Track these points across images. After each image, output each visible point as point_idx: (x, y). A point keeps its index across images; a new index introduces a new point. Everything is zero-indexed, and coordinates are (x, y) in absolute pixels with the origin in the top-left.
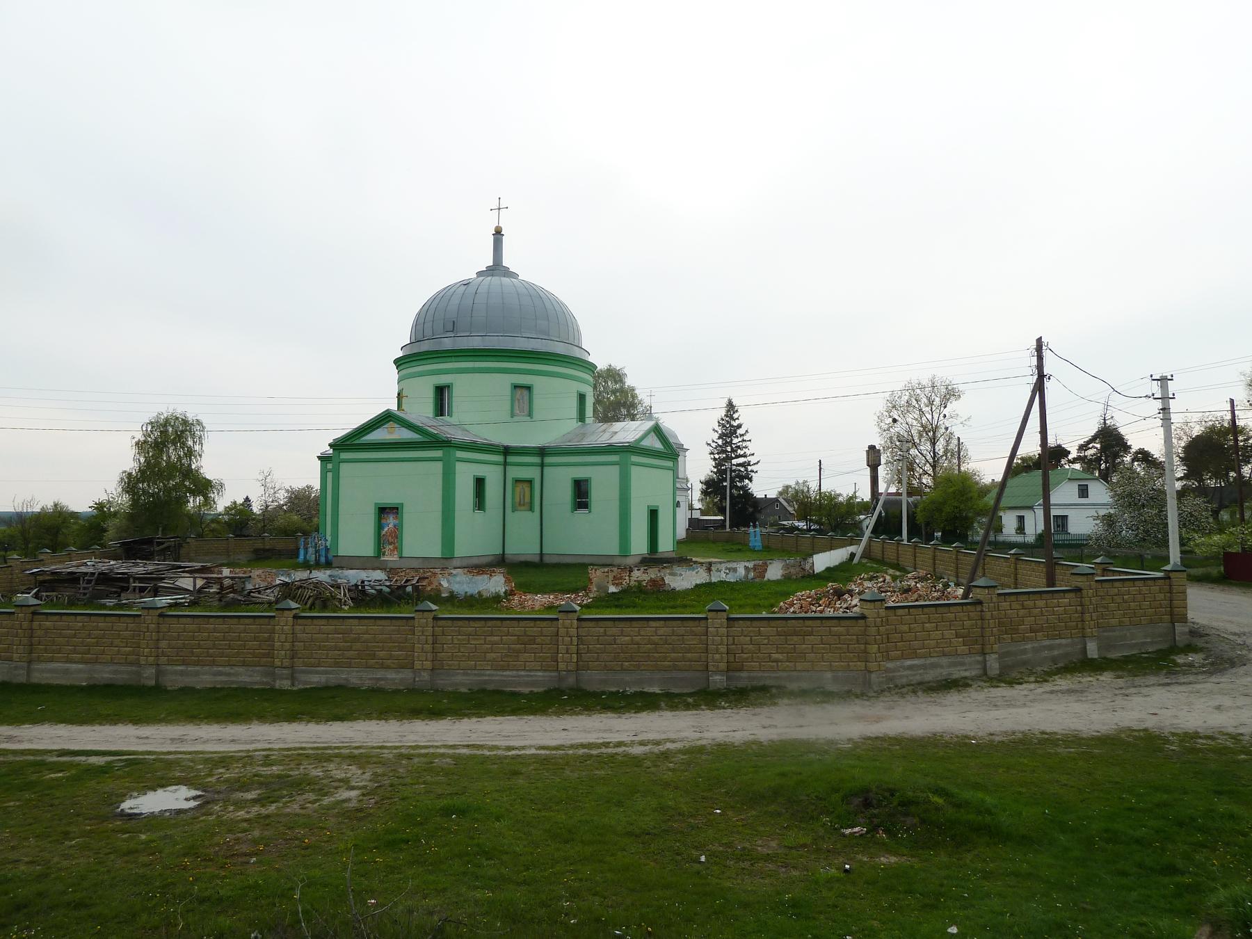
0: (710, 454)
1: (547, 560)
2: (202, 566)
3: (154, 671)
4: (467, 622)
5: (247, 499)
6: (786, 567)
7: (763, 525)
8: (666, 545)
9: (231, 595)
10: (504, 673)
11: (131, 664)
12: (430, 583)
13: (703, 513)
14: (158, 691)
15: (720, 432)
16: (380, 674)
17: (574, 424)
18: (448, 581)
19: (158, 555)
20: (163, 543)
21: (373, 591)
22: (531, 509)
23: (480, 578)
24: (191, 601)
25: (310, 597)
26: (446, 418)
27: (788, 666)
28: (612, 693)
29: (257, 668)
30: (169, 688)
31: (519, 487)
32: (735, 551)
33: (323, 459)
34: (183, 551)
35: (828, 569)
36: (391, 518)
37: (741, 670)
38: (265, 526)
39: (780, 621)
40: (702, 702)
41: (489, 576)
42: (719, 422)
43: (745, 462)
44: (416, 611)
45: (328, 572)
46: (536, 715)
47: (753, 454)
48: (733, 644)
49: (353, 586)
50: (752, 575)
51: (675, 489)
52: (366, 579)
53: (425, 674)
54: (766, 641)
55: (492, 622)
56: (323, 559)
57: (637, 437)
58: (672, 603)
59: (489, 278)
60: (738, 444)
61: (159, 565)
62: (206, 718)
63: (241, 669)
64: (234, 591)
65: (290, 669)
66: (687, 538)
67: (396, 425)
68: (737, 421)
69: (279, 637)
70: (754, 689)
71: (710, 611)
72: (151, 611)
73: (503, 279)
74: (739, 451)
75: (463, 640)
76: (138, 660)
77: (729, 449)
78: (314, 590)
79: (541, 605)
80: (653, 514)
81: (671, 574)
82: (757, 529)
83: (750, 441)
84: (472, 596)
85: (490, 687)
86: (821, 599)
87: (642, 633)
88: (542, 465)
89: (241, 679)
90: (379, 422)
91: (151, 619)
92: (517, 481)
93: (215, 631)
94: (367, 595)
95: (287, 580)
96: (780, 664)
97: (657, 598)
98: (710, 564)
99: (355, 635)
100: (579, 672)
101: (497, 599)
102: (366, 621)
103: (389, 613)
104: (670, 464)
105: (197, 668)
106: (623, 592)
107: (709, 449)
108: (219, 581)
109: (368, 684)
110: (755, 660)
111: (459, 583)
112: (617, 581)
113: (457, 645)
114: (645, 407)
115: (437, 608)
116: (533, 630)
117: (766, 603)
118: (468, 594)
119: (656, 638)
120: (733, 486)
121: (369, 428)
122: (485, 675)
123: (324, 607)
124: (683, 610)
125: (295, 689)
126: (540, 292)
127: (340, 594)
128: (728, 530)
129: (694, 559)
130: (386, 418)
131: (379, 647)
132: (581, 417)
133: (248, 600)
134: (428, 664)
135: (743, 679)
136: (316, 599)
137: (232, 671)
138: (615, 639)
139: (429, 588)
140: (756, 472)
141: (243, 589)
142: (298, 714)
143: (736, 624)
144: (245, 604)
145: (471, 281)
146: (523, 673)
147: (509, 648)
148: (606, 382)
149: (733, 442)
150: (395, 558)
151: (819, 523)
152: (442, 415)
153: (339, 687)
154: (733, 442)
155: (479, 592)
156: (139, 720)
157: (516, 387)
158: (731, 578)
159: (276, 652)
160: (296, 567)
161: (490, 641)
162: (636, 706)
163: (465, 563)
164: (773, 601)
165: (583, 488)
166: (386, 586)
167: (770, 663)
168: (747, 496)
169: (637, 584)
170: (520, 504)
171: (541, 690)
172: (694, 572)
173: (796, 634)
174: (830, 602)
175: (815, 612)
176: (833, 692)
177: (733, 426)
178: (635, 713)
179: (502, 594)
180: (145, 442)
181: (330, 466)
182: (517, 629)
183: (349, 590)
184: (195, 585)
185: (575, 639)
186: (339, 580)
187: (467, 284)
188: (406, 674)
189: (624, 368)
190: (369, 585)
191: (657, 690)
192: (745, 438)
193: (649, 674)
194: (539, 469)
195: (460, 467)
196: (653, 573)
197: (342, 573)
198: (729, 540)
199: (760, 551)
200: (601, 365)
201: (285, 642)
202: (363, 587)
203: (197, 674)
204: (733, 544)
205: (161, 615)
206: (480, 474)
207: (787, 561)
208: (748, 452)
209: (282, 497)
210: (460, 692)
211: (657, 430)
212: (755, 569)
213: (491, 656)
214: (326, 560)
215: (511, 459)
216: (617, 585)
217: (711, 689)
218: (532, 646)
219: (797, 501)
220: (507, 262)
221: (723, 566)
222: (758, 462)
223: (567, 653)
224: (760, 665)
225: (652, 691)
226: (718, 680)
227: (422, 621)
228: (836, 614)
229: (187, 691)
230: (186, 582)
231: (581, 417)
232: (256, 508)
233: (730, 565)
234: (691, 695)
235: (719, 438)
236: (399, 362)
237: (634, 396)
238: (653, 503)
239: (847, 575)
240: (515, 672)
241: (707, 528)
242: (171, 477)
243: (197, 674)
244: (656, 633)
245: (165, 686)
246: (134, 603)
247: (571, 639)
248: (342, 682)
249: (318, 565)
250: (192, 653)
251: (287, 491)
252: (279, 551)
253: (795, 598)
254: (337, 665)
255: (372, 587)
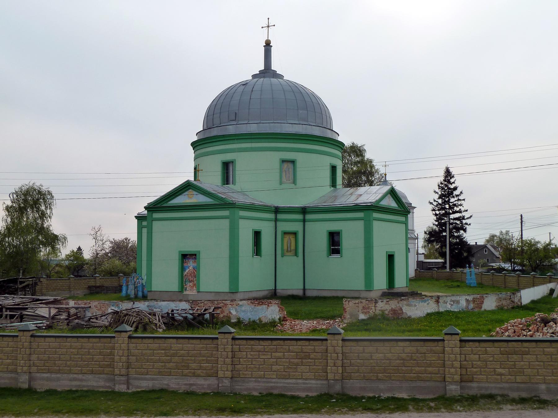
0: (432, 210)
1: (309, 294)
2: (54, 299)
3: (28, 378)
4: (258, 342)
5: (79, 249)
6: (500, 299)
7: (476, 266)
8: (401, 283)
9: (77, 321)
10: (286, 381)
11: (11, 372)
12: (222, 312)
13: (426, 257)
14: (30, 392)
15: (440, 193)
16: (193, 380)
17: (328, 189)
18: (236, 310)
19: (20, 291)
20: (24, 282)
21: (180, 318)
22: (296, 254)
23: (260, 307)
24: (47, 325)
25: (134, 322)
26: (231, 186)
27: (510, 379)
28: (369, 398)
29: (102, 376)
30: (38, 390)
31: (287, 237)
32: (454, 287)
33: (140, 218)
34: (38, 288)
35: (533, 302)
36: (191, 263)
37: (472, 381)
38: (95, 269)
39: (503, 343)
40: (442, 406)
41: (267, 306)
42: (439, 186)
43: (460, 217)
44: (219, 333)
45: (147, 303)
46: (312, 414)
47: (467, 211)
48: (465, 360)
49: (165, 314)
50: (471, 306)
51: (407, 239)
52: (174, 308)
53: (226, 381)
54: (491, 359)
55: (277, 341)
56: (140, 294)
57: (378, 198)
58: (409, 328)
59: (262, 79)
60: (455, 203)
61: (23, 298)
62: (67, 413)
63: (90, 377)
64: (78, 318)
65: (127, 377)
66: (415, 276)
67: (195, 193)
68: (453, 184)
69: (118, 352)
70: (484, 397)
71: (446, 334)
72: (25, 333)
73: (272, 80)
74: (455, 208)
75: (255, 355)
76: (16, 369)
77: (447, 206)
78: (137, 317)
79: (308, 329)
80: (391, 258)
81: (408, 305)
82: (472, 270)
83: (464, 200)
84: (254, 321)
85: (276, 392)
86: (530, 325)
87: (393, 351)
88: (304, 221)
89: (89, 383)
90: (180, 191)
91: (25, 338)
92: (285, 233)
93: (71, 347)
94: (176, 321)
95: (116, 309)
96: (503, 377)
97: (397, 324)
98: (438, 297)
99: (173, 351)
100: (344, 381)
101: (273, 324)
102: (181, 341)
103: (193, 334)
104: (403, 219)
105: (58, 375)
106: (371, 318)
107: (431, 207)
108: (67, 310)
109: (183, 389)
110: (483, 373)
111: (244, 311)
112: (365, 310)
113: (250, 359)
114: (381, 175)
115: (235, 331)
116: (308, 347)
117: (486, 328)
118: (251, 320)
119: (404, 355)
120: (452, 236)
121: (173, 195)
122: (272, 382)
123: (145, 330)
124: (418, 333)
125: (130, 391)
126: (300, 89)
127: (156, 320)
128: (448, 270)
129: (423, 293)
130: (186, 187)
131: (191, 360)
132: (334, 184)
133: (89, 324)
134: (229, 374)
135: (474, 389)
136: (139, 323)
137: (84, 378)
138: (371, 356)
139: (221, 316)
140: (470, 224)
141: (85, 317)
142: (134, 410)
143: (467, 344)
144: (87, 328)
145: (248, 82)
146: (300, 381)
147: (290, 362)
148: (350, 156)
149: (451, 201)
150: (194, 292)
151: (522, 265)
152: (227, 184)
153: (162, 390)
154: (451, 201)
155: (260, 319)
156: (19, 414)
157: (284, 161)
158: (455, 308)
159: (116, 363)
160: (122, 299)
161: (275, 356)
162: (390, 408)
163: (247, 296)
164: (490, 327)
165: (336, 238)
166: (190, 314)
167: (496, 376)
168: (463, 243)
169: (381, 313)
170: (287, 251)
171: (314, 394)
172: (426, 304)
173: (515, 353)
174: (538, 328)
175: (526, 336)
176: (547, 401)
177: (449, 188)
178: (390, 413)
179: (277, 320)
180: (11, 207)
181: (145, 223)
182: (296, 347)
183: (162, 317)
184: (50, 313)
185: (340, 355)
186: (155, 310)
187: (245, 84)
188: (212, 381)
189: (364, 145)
190: (178, 313)
191: (405, 396)
192: (460, 198)
193: (398, 383)
194: (302, 223)
195: (242, 223)
196: (394, 304)
197: (157, 304)
198: (450, 278)
199: (475, 287)
200: (347, 143)
201: (122, 356)
202: (173, 314)
203: (58, 379)
204: (453, 282)
205: (32, 336)
206: (257, 228)
207: (500, 295)
208: (463, 209)
209: (108, 246)
210: (253, 395)
211: (393, 193)
212: (474, 301)
213: (274, 368)
214: (142, 295)
215: (280, 216)
216: (366, 313)
217: (448, 396)
218: (308, 360)
219: (501, 247)
220: (275, 66)
221: (449, 299)
222: (471, 216)
223: (335, 366)
224: (487, 378)
225: (401, 397)
226: (453, 389)
227: (224, 340)
228: (545, 338)
229: (51, 393)
230: (43, 311)
231: (334, 184)
232: (87, 255)
233: (454, 298)
234: (432, 400)
235: (439, 198)
236: (195, 145)
237: (372, 167)
238: (391, 250)
239: (549, 306)
240: (294, 381)
241: (430, 269)
242: (29, 233)
243: (58, 379)
244: (404, 351)
245: (35, 389)
246: (7, 327)
247: (338, 355)
248: (165, 387)
249: (136, 298)
250: (55, 364)
251: (111, 242)
252: (107, 287)
253: (509, 325)
254: (160, 373)
255: (180, 315)
